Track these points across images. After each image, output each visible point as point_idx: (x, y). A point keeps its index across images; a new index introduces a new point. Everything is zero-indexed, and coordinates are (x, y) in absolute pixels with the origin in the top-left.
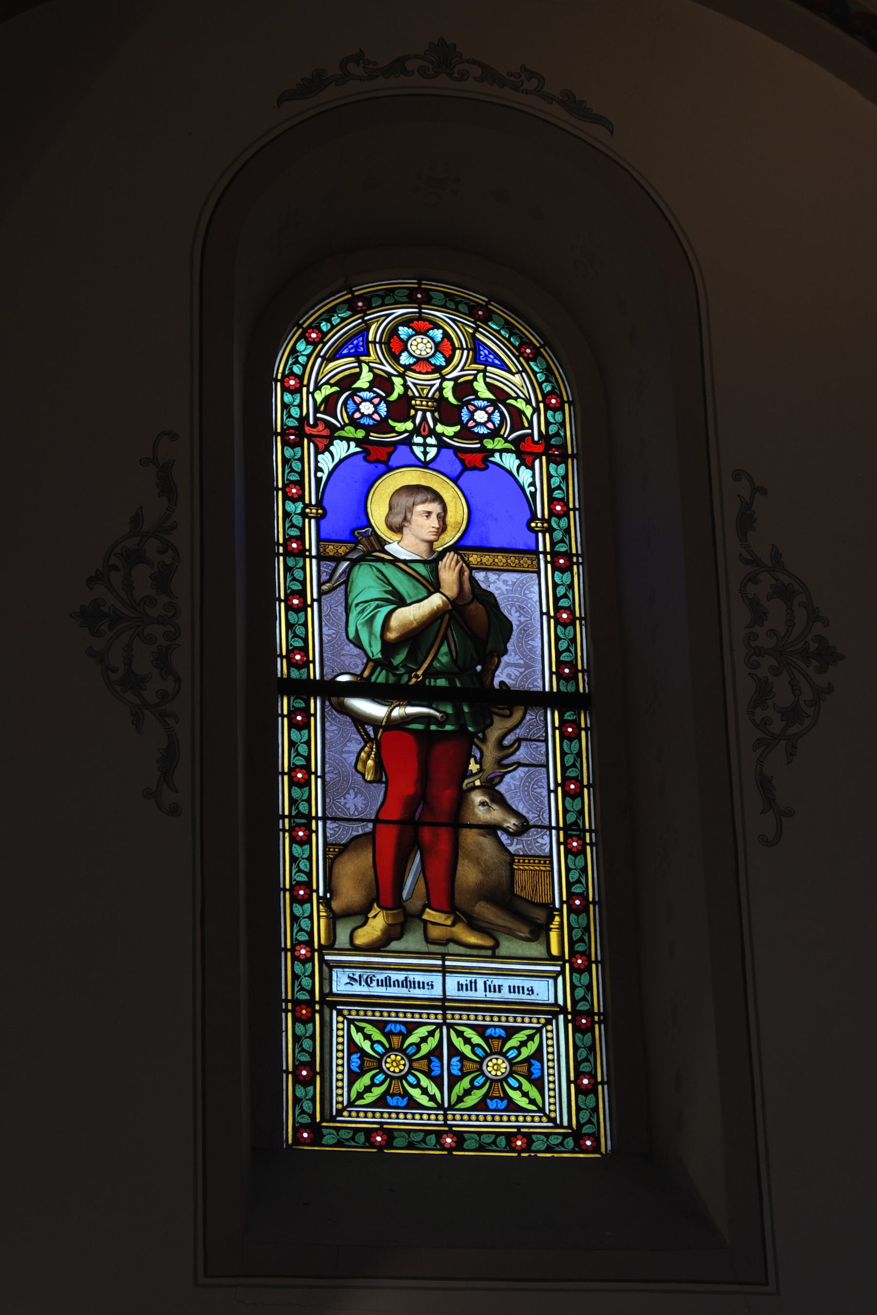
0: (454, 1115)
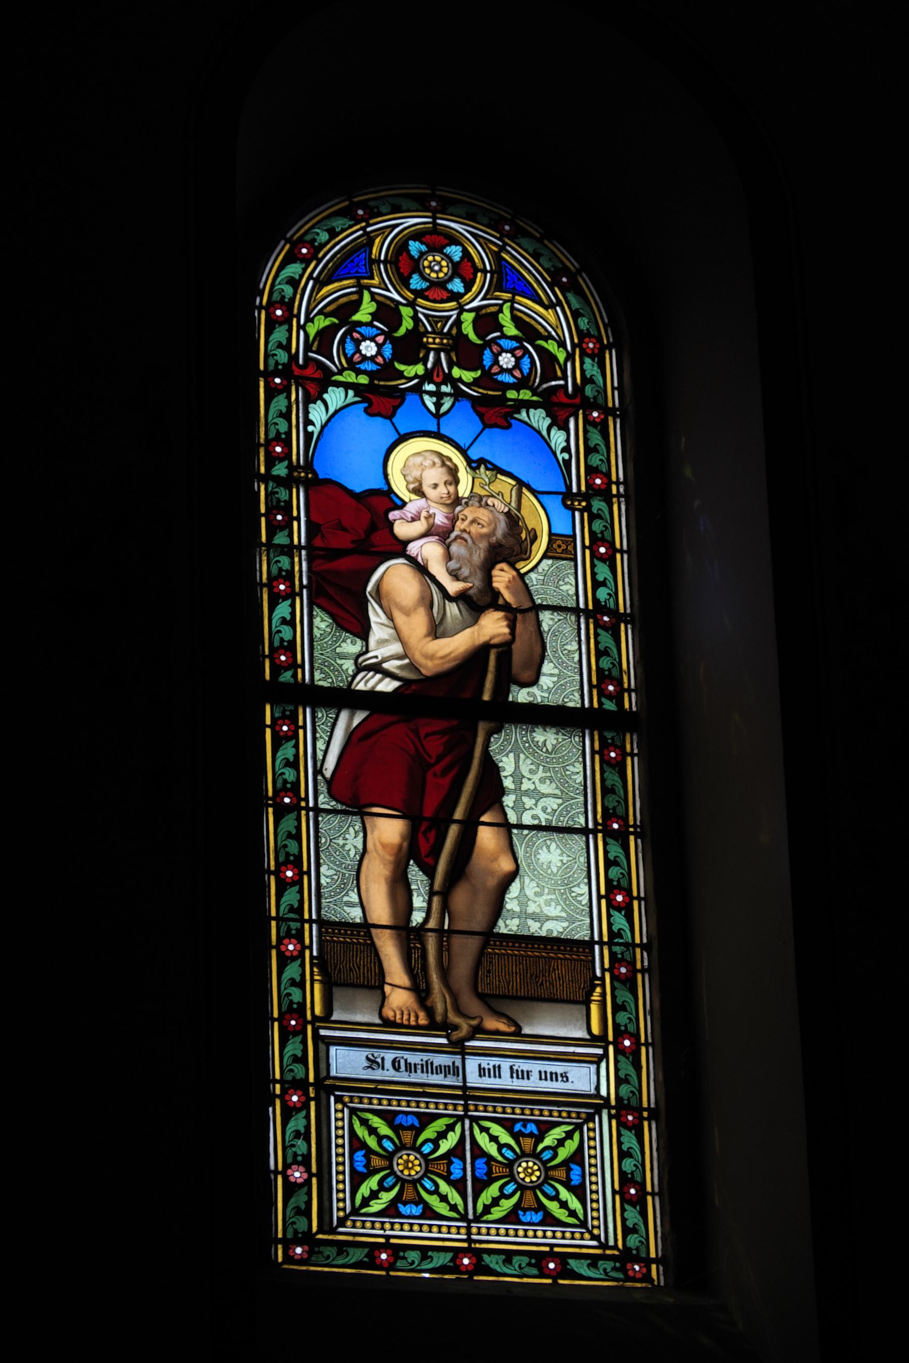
0: (479, 1228)
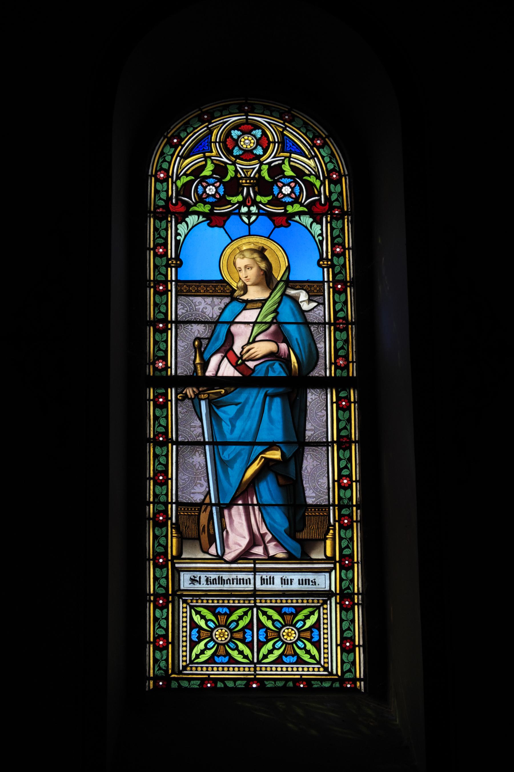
0: (261, 667)
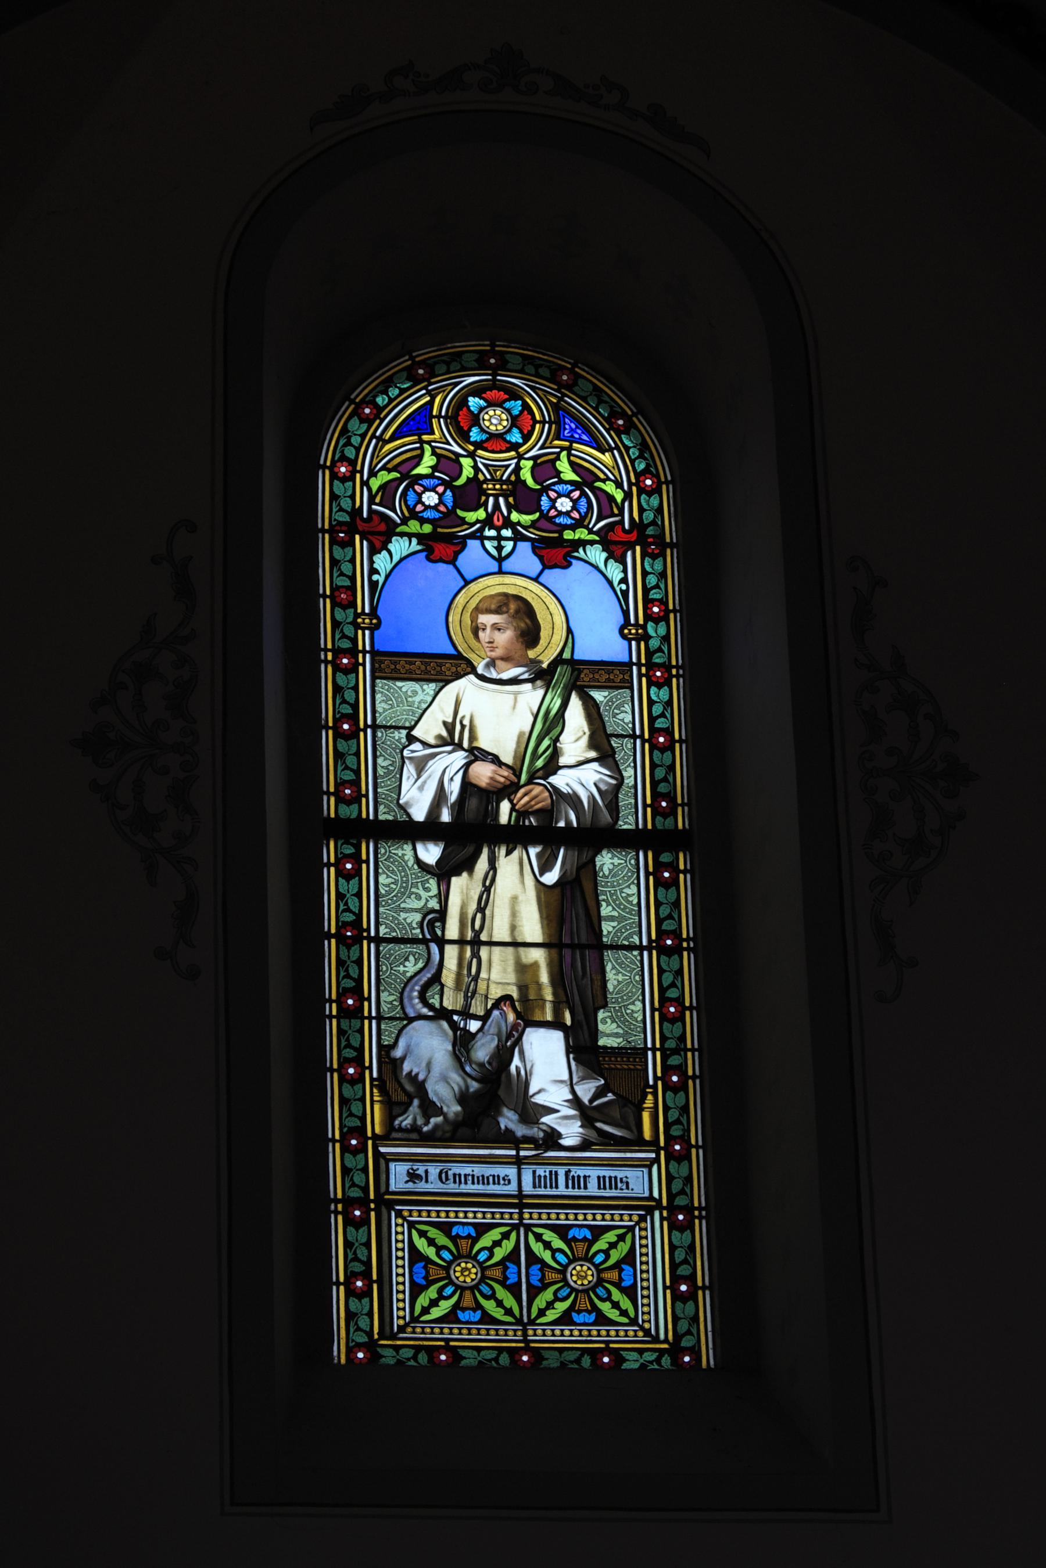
0: (535, 1330)
